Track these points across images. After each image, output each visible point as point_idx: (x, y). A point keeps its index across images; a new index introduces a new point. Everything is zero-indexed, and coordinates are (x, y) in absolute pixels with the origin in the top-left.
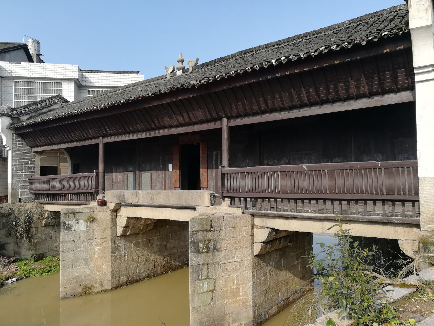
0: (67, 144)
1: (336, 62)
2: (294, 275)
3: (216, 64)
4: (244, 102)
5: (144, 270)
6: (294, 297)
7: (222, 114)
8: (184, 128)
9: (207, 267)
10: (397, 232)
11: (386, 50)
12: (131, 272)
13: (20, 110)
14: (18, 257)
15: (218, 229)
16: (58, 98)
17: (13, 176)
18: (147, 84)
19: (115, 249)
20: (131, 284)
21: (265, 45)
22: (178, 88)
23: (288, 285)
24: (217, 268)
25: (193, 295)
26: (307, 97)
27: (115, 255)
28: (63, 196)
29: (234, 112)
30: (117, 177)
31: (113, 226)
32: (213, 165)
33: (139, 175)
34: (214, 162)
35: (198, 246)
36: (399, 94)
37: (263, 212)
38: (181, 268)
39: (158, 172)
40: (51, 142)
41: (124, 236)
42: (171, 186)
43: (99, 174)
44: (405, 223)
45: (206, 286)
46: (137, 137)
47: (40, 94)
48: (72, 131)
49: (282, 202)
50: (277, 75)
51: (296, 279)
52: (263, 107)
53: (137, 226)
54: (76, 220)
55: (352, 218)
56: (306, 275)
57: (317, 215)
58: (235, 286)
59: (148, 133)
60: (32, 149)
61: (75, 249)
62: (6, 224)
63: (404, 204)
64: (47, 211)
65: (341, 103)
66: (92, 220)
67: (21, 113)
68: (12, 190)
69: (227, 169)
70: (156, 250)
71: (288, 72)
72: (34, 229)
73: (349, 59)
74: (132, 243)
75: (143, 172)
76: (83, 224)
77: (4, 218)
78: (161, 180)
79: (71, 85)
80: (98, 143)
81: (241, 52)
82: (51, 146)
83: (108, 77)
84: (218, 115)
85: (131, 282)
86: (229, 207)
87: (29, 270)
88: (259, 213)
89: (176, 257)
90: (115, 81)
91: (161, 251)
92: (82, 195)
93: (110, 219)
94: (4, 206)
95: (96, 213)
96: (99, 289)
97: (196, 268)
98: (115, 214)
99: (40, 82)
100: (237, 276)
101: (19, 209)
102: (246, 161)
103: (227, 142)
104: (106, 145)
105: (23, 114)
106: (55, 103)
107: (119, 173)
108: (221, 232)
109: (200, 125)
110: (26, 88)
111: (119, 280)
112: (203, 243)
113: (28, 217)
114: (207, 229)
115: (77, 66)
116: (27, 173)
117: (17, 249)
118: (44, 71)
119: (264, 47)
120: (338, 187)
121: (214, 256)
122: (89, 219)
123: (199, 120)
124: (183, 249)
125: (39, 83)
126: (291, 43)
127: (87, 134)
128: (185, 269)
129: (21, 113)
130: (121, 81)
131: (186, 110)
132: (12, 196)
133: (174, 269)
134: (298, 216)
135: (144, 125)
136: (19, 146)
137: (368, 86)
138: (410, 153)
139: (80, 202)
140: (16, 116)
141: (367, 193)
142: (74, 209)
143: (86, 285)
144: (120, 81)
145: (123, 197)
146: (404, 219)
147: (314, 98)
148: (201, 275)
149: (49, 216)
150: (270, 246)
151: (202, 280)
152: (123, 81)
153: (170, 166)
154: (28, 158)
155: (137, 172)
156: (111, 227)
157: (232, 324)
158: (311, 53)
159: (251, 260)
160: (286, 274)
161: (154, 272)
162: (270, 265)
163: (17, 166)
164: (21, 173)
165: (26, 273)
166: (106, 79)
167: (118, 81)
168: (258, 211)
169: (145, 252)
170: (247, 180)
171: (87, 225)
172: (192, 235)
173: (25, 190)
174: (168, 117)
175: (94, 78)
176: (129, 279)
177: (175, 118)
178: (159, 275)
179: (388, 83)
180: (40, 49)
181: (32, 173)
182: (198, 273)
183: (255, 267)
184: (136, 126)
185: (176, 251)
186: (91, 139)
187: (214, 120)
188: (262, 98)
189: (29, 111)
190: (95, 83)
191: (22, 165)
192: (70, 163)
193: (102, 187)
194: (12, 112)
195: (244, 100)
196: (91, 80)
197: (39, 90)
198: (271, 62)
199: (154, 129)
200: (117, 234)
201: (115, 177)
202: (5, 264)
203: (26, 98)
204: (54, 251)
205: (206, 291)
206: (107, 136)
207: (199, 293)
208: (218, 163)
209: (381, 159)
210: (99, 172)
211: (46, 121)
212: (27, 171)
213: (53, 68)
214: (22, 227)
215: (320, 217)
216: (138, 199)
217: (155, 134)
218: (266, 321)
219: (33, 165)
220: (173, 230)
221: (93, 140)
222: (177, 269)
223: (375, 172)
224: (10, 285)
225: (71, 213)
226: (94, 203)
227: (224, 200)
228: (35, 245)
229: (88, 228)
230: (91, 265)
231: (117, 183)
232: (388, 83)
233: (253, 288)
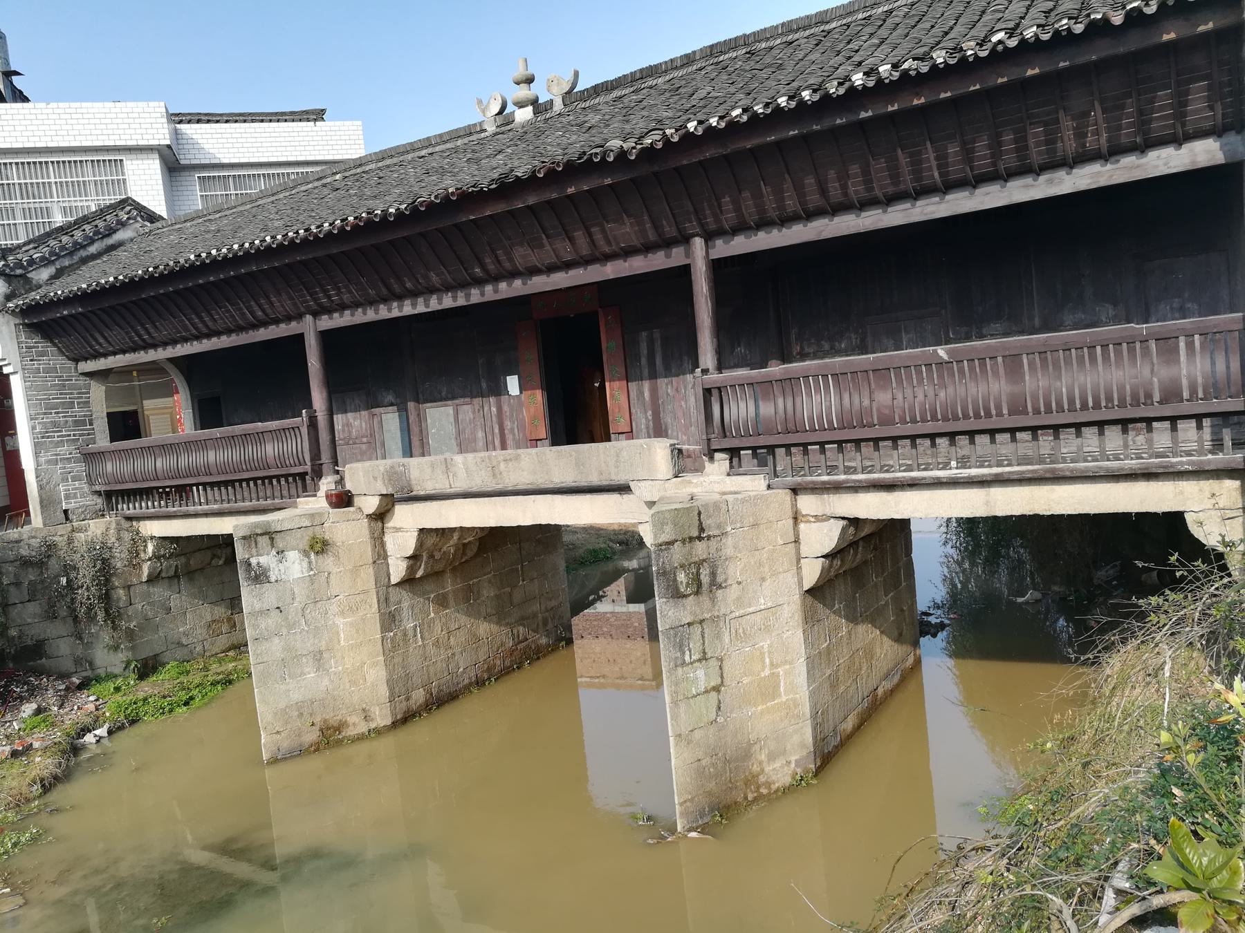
0: (195, 343)
1: (1030, 72)
2: (882, 632)
3: (637, 85)
4: (761, 189)
5: (465, 664)
6: (886, 688)
7: (692, 226)
8: (572, 272)
9: (700, 630)
10: (1182, 493)
11: (1169, 34)
12: (436, 675)
13: (26, 251)
14: (89, 673)
15: (716, 532)
16: (129, 208)
17: (38, 448)
18: (423, 153)
19: (389, 620)
20: (438, 707)
21: (783, 24)
22: (570, 162)
23: (872, 658)
24: (724, 629)
25: (675, 703)
26: (939, 167)
27: (392, 634)
28: (168, 494)
29: (729, 218)
30: (347, 425)
31: (378, 559)
32: (640, 369)
33: (419, 415)
34: (644, 361)
35: (675, 580)
36: (1187, 148)
37: (825, 478)
38: (552, 650)
39: (477, 401)
40: (144, 340)
41: (409, 581)
42: (521, 435)
43: (316, 420)
44: (1206, 468)
45: (701, 677)
46: (427, 306)
47: (61, 199)
48: (216, 304)
49: (841, 449)
50: (863, 115)
51: (887, 642)
52: (814, 199)
53: (440, 551)
54: (278, 553)
55: (1068, 470)
56: (904, 632)
57: (974, 472)
58: (767, 672)
59: (460, 294)
60: (77, 364)
61: (284, 631)
62: (39, 587)
63: (1081, 432)
64: (152, 539)
65: (1029, 180)
66: (320, 547)
67: (31, 262)
68: (41, 489)
69: (714, 377)
70: (489, 610)
71: (893, 106)
72: (121, 592)
73: (1067, 63)
74: (428, 599)
75: (429, 405)
76: (298, 561)
77: (30, 570)
78: (488, 423)
79: (151, 166)
80: (303, 334)
81: (712, 47)
82: (142, 352)
83: (256, 135)
84: (679, 230)
85: (440, 701)
86: (728, 475)
87: (135, 703)
88: (813, 482)
89: (538, 625)
90: (278, 144)
91: (499, 615)
92: (241, 486)
93: (369, 541)
94: (25, 536)
95: (330, 526)
96: (362, 728)
97: (676, 635)
98: (380, 524)
99: (52, 162)
100: (770, 646)
101: (70, 541)
102: (740, 350)
103: (710, 304)
104: (327, 338)
105: (35, 263)
106: (123, 224)
107: (351, 412)
108: (724, 541)
109: (622, 261)
110: (14, 184)
111: (408, 699)
112: (685, 572)
113: (98, 560)
114: (691, 535)
115: (162, 104)
116: (74, 435)
117: (79, 651)
118: (64, 127)
119: (780, 32)
120: (961, 401)
121: (713, 600)
122: (312, 547)
123: (622, 249)
124: (553, 601)
125: (14, 165)
126: (860, 16)
127: (263, 311)
128: (563, 653)
129: (31, 262)
130: (297, 144)
131: (583, 223)
132: (42, 507)
133: (535, 655)
134: (924, 478)
135: (449, 272)
136: (40, 360)
137: (1109, 130)
138: (1186, 295)
139: (269, 501)
140: (19, 272)
141: (1110, 405)
142: (268, 522)
143: (325, 721)
144: (293, 144)
145: (404, 478)
146: (1205, 460)
147: (956, 168)
148: (687, 653)
149: (159, 551)
150: (839, 563)
151: (692, 663)
152: (302, 143)
153: (513, 383)
154: (71, 394)
155: (411, 405)
156: (374, 562)
157: (769, 764)
158: (965, 51)
159: (799, 602)
160: (867, 632)
161: (489, 669)
162: (834, 613)
163: (43, 419)
164: (58, 437)
165: (129, 711)
166: (249, 140)
167: (288, 144)
168: (809, 478)
169: (463, 619)
170: (780, 401)
171: (310, 563)
172: (659, 554)
173: (74, 485)
174: (528, 244)
175: (215, 141)
176: (432, 694)
177: (548, 247)
178: (502, 675)
179: (1160, 121)
180: (7, 55)
181: (89, 434)
182: (681, 647)
183: (809, 619)
184: (426, 277)
185: (536, 607)
186: (276, 322)
187: (667, 244)
188: (810, 177)
189: (52, 253)
190: (218, 156)
191: (58, 413)
192: (189, 396)
193: (330, 456)
194: (6, 260)
195: (760, 185)
196: (206, 146)
197: (54, 186)
198: (850, 80)
199: (479, 282)
200: (389, 579)
201: (343, 426)
202: (60, 696)
203: (18, 213)
204: (183, 645)
205: (703, 690)
206: (329, 311)
207: (688, 698)
208: (657, 363)
209: (1110, 316)
210: (317, 414)
211: (137, 279)
212: (74, 430)
213: (89, 116)
214: (88, 589)
215: (983, 475)
216: (451, 477)
217: (482, 294)
218: (838, 748)
219: (88, 411)
220: (523, 552)
221: (283, 326)
222: (544, 656)
223: (1132, 351)
224: (94, 747)
225: (262, 535)
226: (311, 502)
227: (711, 459)
228: (130, 634)
229: (312, 570)
230: (333, 669)
231: (351, 442)
232: (1160, 121)
233: (808, 672)
